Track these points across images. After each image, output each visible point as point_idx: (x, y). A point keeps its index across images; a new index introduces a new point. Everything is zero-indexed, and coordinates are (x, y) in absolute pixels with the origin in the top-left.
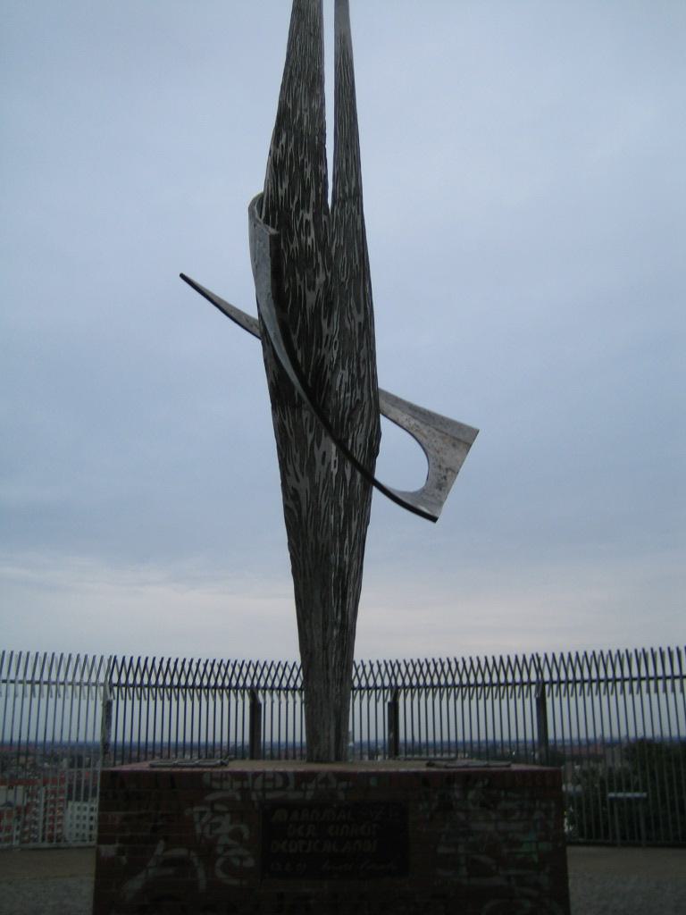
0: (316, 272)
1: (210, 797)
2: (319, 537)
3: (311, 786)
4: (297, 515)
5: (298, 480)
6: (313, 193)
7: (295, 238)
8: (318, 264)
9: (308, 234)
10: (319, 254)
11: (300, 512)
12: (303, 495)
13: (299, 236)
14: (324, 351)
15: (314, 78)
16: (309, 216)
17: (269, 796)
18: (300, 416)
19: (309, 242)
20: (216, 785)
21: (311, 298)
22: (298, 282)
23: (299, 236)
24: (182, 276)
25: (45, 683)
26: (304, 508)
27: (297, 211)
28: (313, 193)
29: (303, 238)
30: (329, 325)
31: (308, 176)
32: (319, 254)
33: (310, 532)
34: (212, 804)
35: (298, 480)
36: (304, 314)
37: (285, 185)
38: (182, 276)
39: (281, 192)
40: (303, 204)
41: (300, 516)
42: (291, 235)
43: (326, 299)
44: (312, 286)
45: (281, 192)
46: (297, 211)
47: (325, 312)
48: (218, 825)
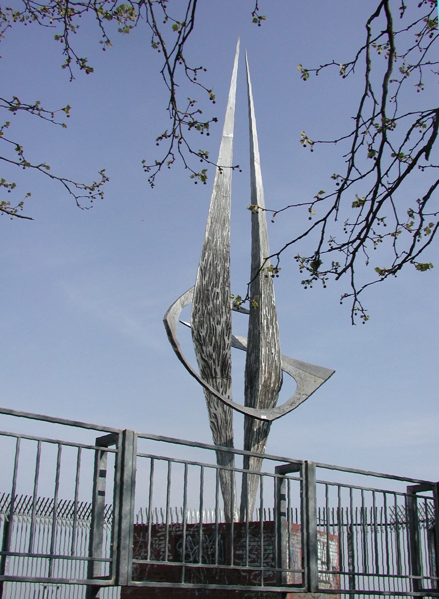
0: (221, 316)
1: (159, 534)
2: (227, 433)
3: (192, 529)
4: (216, 424)
5: (216, 410)
6: (221, 278)
7: (211, 302)
8: (223, 312)
9: (217, 298)
10: (224, 307)
11: (217, 423)
12: (218, 416)
13: (213, 300)
14: (227, 351)
15: (224, 220)
16: (218, 290)
17: (178, 533)
18: (216, 382)
19: (218, 303)
20: (160, 530)
21: (219, 328)
22: (212, 323)
23: (213, 300)
24: (401, 17)
25: (383, 525)
26: (220, 421)
27: (212, 289)
28: (221, 278)
29: (215, 301)
30: (228, 339)
31: (219, 270)
32: (224, 307)
33: (223, 431)
34: (159, 537)
35: (216, 410)
36: (215, 337)
37: (207, 279)
38: (401, 17)
39: (204, 283)
40: (216, 285)
41: (218, 425)
42: (209, 300)
43: (227, 327)
44: (219, 323)
45: (204, 283)
46: (212, 289)
47: (227, 333)
48: (161, 544)
